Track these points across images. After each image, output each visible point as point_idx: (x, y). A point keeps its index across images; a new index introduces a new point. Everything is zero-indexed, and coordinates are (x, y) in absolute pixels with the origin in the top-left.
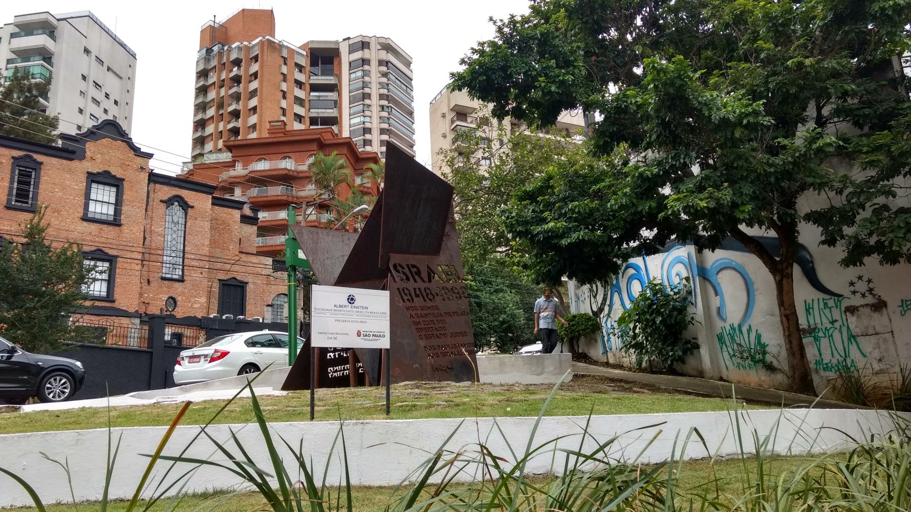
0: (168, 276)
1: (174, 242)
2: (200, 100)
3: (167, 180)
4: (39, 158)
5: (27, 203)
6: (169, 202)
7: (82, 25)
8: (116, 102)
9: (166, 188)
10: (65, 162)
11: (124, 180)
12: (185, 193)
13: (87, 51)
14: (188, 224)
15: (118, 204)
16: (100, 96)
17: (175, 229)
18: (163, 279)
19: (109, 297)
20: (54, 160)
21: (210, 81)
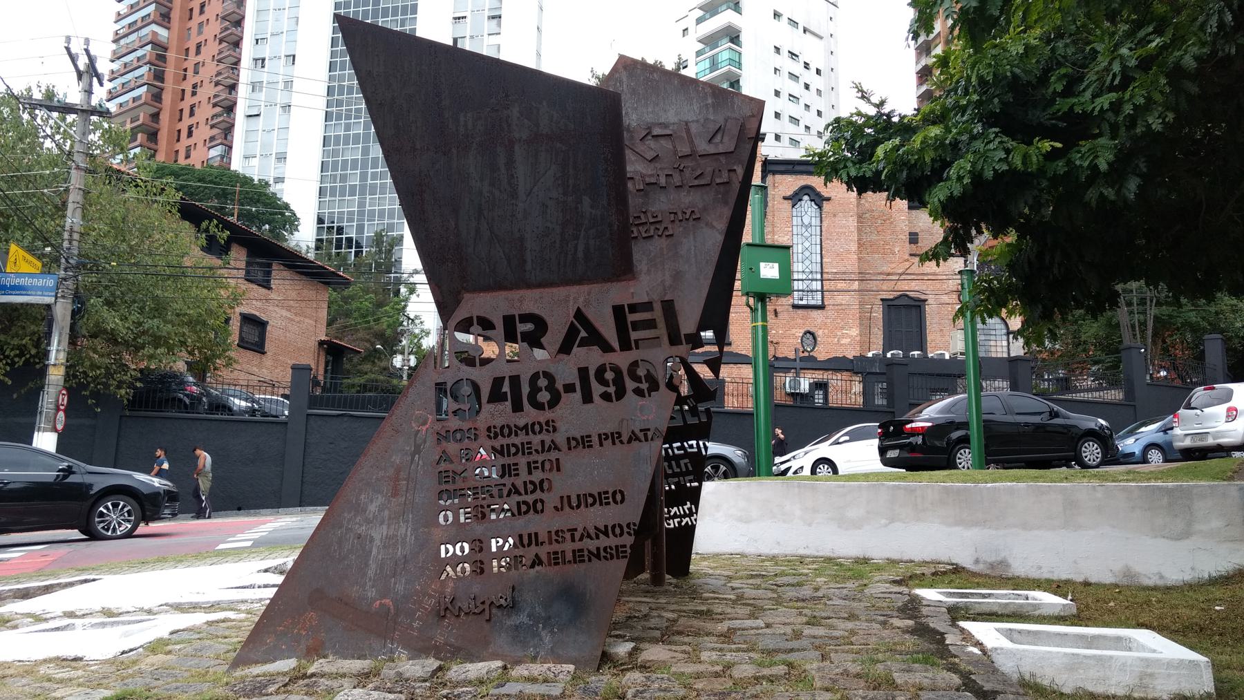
1: (807, 254)
6: (795, 198)
8: (818, 72)
9: (789, 179)
14: (825, 224)
16: (798, 68)
17: (806, 234)
18: (795, 307)
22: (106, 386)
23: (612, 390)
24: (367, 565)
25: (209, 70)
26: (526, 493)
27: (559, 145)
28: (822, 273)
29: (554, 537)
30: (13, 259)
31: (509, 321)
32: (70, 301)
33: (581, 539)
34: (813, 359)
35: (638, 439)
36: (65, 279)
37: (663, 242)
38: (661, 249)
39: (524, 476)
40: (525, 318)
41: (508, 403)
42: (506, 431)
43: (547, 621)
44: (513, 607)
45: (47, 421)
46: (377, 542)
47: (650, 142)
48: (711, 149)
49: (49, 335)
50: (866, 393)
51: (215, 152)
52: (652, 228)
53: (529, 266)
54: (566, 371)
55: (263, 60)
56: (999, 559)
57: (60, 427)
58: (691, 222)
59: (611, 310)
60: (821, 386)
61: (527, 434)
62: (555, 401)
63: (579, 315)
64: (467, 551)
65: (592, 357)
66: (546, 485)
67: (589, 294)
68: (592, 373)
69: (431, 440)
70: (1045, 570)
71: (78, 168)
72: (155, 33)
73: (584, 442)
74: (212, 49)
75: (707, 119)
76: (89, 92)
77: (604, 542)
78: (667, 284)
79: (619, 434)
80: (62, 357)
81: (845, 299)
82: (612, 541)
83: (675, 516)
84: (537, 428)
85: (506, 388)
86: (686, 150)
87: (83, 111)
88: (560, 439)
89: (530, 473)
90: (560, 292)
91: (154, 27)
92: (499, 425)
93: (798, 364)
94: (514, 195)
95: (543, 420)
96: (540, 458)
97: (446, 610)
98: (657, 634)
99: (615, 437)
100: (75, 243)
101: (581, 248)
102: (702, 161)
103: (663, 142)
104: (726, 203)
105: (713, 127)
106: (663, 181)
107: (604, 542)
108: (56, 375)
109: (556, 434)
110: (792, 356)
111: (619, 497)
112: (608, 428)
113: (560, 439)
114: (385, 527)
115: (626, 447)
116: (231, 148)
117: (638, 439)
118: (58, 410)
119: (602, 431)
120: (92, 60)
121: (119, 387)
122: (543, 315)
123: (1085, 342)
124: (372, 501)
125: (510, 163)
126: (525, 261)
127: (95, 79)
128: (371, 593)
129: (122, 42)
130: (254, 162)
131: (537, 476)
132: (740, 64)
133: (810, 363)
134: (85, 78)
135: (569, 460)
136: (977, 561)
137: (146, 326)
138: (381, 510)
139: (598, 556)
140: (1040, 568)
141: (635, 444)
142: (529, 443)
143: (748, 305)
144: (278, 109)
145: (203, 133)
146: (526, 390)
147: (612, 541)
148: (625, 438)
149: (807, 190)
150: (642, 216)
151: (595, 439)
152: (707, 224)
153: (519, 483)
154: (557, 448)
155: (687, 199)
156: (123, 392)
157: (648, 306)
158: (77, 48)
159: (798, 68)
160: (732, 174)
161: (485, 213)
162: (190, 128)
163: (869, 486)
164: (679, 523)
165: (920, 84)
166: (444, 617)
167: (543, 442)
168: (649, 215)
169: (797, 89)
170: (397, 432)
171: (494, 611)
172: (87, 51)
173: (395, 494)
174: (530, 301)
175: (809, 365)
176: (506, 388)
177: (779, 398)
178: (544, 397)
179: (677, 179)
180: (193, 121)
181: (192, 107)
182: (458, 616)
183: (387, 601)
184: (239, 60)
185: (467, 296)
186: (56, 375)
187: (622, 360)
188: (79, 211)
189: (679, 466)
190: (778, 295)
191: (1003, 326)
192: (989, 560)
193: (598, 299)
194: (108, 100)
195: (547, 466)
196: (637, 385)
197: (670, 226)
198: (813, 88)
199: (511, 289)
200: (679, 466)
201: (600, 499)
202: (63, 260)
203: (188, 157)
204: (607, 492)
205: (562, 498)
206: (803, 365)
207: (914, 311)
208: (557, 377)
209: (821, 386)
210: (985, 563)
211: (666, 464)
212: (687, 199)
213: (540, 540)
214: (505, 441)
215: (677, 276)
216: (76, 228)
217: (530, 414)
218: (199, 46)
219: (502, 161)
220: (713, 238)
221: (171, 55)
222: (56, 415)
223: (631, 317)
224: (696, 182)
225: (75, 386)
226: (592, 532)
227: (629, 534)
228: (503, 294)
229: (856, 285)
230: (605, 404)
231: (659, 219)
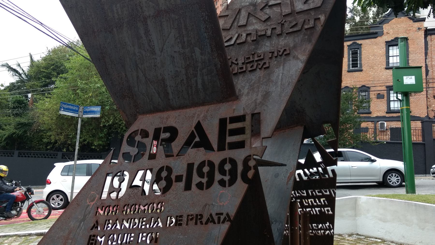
4: (359, 42)
5: (357, 67)
10: (373, 40)
15: (388, 57)
20: (367, 41)
27: (173, 16)
38: (260, 77)
40: (167, 129)
47: (268, 11)
48: (306, 7)
53: (171, 96)
58: (284, 57)
68: (195, 167)
78: (258, 101)
79: (201, 215)
94: (153, 52)
102: (298, 17)
103: (275, 9)
104: (310, 41)
112: (195, 211)
122: (177, 128)
125: (147, 32)
126: (168, 93)
141: (211, 225)
148: (204, 220)
152: (294, 57)
157: (241, 118)
161: (140, 66)
164: (324, 233)
174: (172, 118)
179: (278, 31)
190: (415, 92)
193: (210, 117)
208: (174, 170)
212: (283, 42)
224: (291, 30)
228: (159, 114)
230: (198, 191)
231: (262, 57)
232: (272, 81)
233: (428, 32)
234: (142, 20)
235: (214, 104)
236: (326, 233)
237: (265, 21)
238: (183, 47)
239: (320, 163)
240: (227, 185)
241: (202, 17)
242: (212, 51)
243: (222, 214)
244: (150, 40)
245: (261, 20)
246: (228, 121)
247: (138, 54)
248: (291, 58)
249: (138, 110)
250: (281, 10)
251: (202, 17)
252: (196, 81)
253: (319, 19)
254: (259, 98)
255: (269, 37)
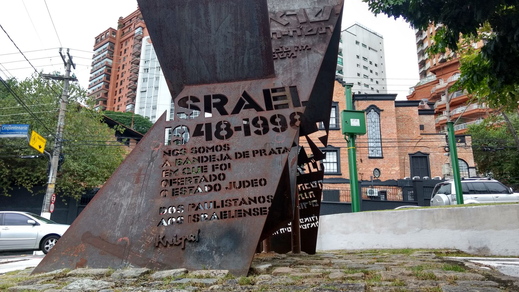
0: (373, 156)
2: (420, 49)
3: (368, 98)
7: (353, 30)
8: (376, 65)
9: (364, 102)
11: (338, 102)
12: (376, 103)
13: (357, 43)
14: (381, 121)
16: (367, 64)
17: (374, 126)
18: (370, 158)
19: (339, 173)
21: (424, 36)
22: (70, 193)
23: (261, 129)
24: (117, 219)
25: (127, 75)
26: (211, 181)
27: (232, 3)
28: (381, 139)
29: (225, 203)
30: (33, 138)
31: (207, 99)
32: (58, 157)
33: (240, 205)
34: (379, 181)
35: (275, 153)
36: (56, 148)
37: (291, 60)
39: (210, 172)
40: (215, 97)
41: (204, 137)
42: (202, 150)
43: (218, 250)
44: (198, 241)
45: (47, 208)
46: (125, 207)
47: (285, 18)
48: (317, 19)
49: (49, 171)
50: (404, 195)
51: (129, 107)
52: (285, 54)
53: (218, 70)
54: (236, 120)
55: (148, 69)
56: (483, 246)
57: (52, 210)
59: (262, 92)
60: (381, 193)
61: (213, 151)
62: (230, 134)
63: (245, 94)
64: (175, 211)
65: (252, 114)
66: (222, 177)
67: (251, 85)
69: (160, 155)
70: (509, 251)
71: (63, 102)
72: (107, 62)
73: (245, 155)
74: (128, 67)
75: (315, 8)
76: (69, 71)
77: (253, 206)
78: (293, 79)
79: (264, 151)
80: (54, 180)
81: (392, 154)
82: (258, 205)
83: (307, 222)
84: (219, 148)
85: (203, 129)
86: (303, 20)
87: (66, 79)
88: (231, 153)
89: (213, 170)
90: (237, 84)
91: (107, 60)
92: (198, 147)
93: (372, 183)
94: (209, 31)
95: (222, 144)
96: (220, 163)
97: (161, 243)
98: (288, 264)
99: (262, 152)
100: (61, 133)
101: (246, 59)
102: (312, 25)
103: (292, 18)
104: (325, 42)
105: (317, 10)
106: (291, 33)
107: (253, 206)
108: (51, 188)
109: (229, 151)
110: (369, 179)
111: (263, 182)
112: (258, 148)
113: (231, 153)
114: (130, 199)
115: (268, 157)
116: (135, 105)
117: (275, 153)
118: (51, 203)
119: (254, 149)
120: (70, 58)
121: (76, 194)
122: (225, 95)
123: (505, 174)
124: (124, 186)
125: (206, 13)
126: (216, 67)
127: (72, 66)
128: (118, 234)
129: (95, 66)
130: (144, 110)
131: (217, 172)
132: (342, 63)
133: (377, 183)
134: (68, 65)
135: (236, 164)
136: (470, 248)
137: (88, 168)
138: (129, 190)
139: (250, 214)
140: (507, 250)
141: (273, 155)
142: (215, 156)
143: (346, 139)
144: (154, 89)
145: (124, 99)
146: (214, 130)
147: (258, 205)
148: (268, 152)
149: (373, 107)
150: (280, 49)
151: (251, 153)
152: (314, 51)
153: (207, 175)
154: (229, 158)
155: (303, 41)
156: (77, 196)
157: (283, 89)
158: (64, 53)
159: (367, 64)
160: (327, 30)
161: (194, 41)
162: (119, 98)
163: (409, 211)
164: (310, 226)
165: (420, 68)
166: (158, 247)
167: (222, 155)
168: (284, 48)
169: (367, 72)
170: (142, 151)
171: (187, 243)
172: (68, 53)
173: (138, 181)
174: (219, 89)
175: (377, 184)
176: (203, 129)
177: (364, 196)
178: (224, 133)
179: (299, 32)
180: (120, 95)
181: (120, 89)
182: (166, 246)
183: (126, 238)
184: (138, 71)
185: (186, 87)
186: (51, 188)
187: (268, 115)
188: (63, 119)
189: (308, 195)
190: (360, 134)
191: (465, 165)
192: (477, 247)
193: (256, 90)
194: (89, 89)
195: (223, 167)
196: (275, 126)
197: (295, 53)
198: (374, 72)
199: (209, 83)
200: (308, 195)
201: (253, 183)
202: (56, 140)
203: (118, 109)
204: (256, 180)
205: (231, 183)
206: (375, 183)
207: (424, 159)
209: (384, 193)
210: (475, 248)
211: (301, 195)
212: (303, 41)
213: (217, 205)
214: (200, 155)
215: (298, 75)
216: (62, 126)
217: (216, 141)
218: (123, 66)
219: (202, 12)
220: (316, 58)
221: (113, 70)
222: (50, 205)
223: (273, 95)
224: (309, 33)
225: (59, 193)
226: (247, 200)
227: (268, 201)
228: (205, 86)
229: (396, 144)
230: (257, 136)
231: (289, 50)
232: (301, 66)
233: (356, 98)
234: (204, 3)
235: (255, 79)
236: (311, 226)
237: (285, 26)
238: (236, 30)
239: (311, 158)
240: (280, 131)
241: (256, 7)
242: (260, 35)
243: (281, 148)
244: (208, 20)
245: (282, 25)
246: (271, 91)
247: (195, 31)
248: (312, 51)
249: (185, 81)
250: (298, 19)
251: (256, 7)
252: (243, 59)
253: (329, 28)
254: (293, 77)
255: (292, 37)
